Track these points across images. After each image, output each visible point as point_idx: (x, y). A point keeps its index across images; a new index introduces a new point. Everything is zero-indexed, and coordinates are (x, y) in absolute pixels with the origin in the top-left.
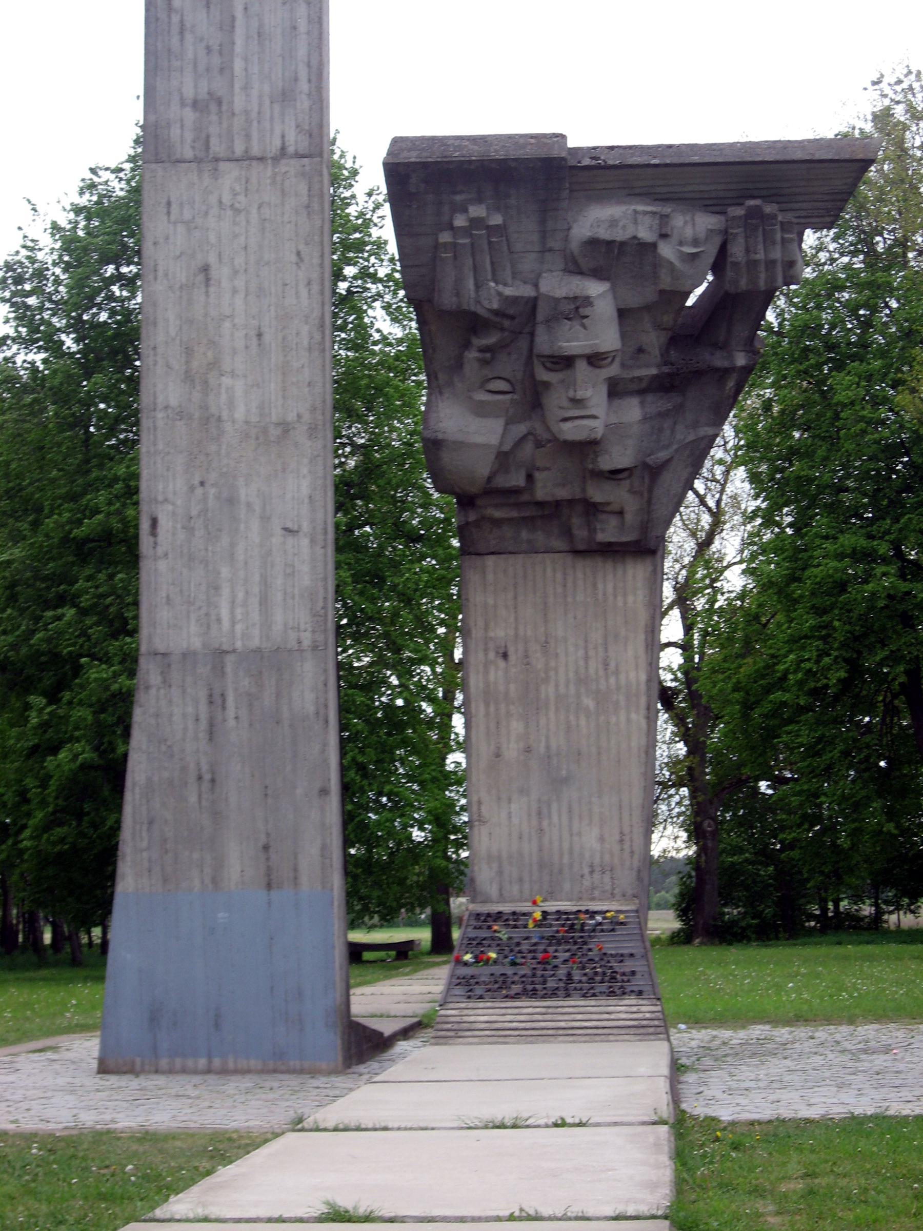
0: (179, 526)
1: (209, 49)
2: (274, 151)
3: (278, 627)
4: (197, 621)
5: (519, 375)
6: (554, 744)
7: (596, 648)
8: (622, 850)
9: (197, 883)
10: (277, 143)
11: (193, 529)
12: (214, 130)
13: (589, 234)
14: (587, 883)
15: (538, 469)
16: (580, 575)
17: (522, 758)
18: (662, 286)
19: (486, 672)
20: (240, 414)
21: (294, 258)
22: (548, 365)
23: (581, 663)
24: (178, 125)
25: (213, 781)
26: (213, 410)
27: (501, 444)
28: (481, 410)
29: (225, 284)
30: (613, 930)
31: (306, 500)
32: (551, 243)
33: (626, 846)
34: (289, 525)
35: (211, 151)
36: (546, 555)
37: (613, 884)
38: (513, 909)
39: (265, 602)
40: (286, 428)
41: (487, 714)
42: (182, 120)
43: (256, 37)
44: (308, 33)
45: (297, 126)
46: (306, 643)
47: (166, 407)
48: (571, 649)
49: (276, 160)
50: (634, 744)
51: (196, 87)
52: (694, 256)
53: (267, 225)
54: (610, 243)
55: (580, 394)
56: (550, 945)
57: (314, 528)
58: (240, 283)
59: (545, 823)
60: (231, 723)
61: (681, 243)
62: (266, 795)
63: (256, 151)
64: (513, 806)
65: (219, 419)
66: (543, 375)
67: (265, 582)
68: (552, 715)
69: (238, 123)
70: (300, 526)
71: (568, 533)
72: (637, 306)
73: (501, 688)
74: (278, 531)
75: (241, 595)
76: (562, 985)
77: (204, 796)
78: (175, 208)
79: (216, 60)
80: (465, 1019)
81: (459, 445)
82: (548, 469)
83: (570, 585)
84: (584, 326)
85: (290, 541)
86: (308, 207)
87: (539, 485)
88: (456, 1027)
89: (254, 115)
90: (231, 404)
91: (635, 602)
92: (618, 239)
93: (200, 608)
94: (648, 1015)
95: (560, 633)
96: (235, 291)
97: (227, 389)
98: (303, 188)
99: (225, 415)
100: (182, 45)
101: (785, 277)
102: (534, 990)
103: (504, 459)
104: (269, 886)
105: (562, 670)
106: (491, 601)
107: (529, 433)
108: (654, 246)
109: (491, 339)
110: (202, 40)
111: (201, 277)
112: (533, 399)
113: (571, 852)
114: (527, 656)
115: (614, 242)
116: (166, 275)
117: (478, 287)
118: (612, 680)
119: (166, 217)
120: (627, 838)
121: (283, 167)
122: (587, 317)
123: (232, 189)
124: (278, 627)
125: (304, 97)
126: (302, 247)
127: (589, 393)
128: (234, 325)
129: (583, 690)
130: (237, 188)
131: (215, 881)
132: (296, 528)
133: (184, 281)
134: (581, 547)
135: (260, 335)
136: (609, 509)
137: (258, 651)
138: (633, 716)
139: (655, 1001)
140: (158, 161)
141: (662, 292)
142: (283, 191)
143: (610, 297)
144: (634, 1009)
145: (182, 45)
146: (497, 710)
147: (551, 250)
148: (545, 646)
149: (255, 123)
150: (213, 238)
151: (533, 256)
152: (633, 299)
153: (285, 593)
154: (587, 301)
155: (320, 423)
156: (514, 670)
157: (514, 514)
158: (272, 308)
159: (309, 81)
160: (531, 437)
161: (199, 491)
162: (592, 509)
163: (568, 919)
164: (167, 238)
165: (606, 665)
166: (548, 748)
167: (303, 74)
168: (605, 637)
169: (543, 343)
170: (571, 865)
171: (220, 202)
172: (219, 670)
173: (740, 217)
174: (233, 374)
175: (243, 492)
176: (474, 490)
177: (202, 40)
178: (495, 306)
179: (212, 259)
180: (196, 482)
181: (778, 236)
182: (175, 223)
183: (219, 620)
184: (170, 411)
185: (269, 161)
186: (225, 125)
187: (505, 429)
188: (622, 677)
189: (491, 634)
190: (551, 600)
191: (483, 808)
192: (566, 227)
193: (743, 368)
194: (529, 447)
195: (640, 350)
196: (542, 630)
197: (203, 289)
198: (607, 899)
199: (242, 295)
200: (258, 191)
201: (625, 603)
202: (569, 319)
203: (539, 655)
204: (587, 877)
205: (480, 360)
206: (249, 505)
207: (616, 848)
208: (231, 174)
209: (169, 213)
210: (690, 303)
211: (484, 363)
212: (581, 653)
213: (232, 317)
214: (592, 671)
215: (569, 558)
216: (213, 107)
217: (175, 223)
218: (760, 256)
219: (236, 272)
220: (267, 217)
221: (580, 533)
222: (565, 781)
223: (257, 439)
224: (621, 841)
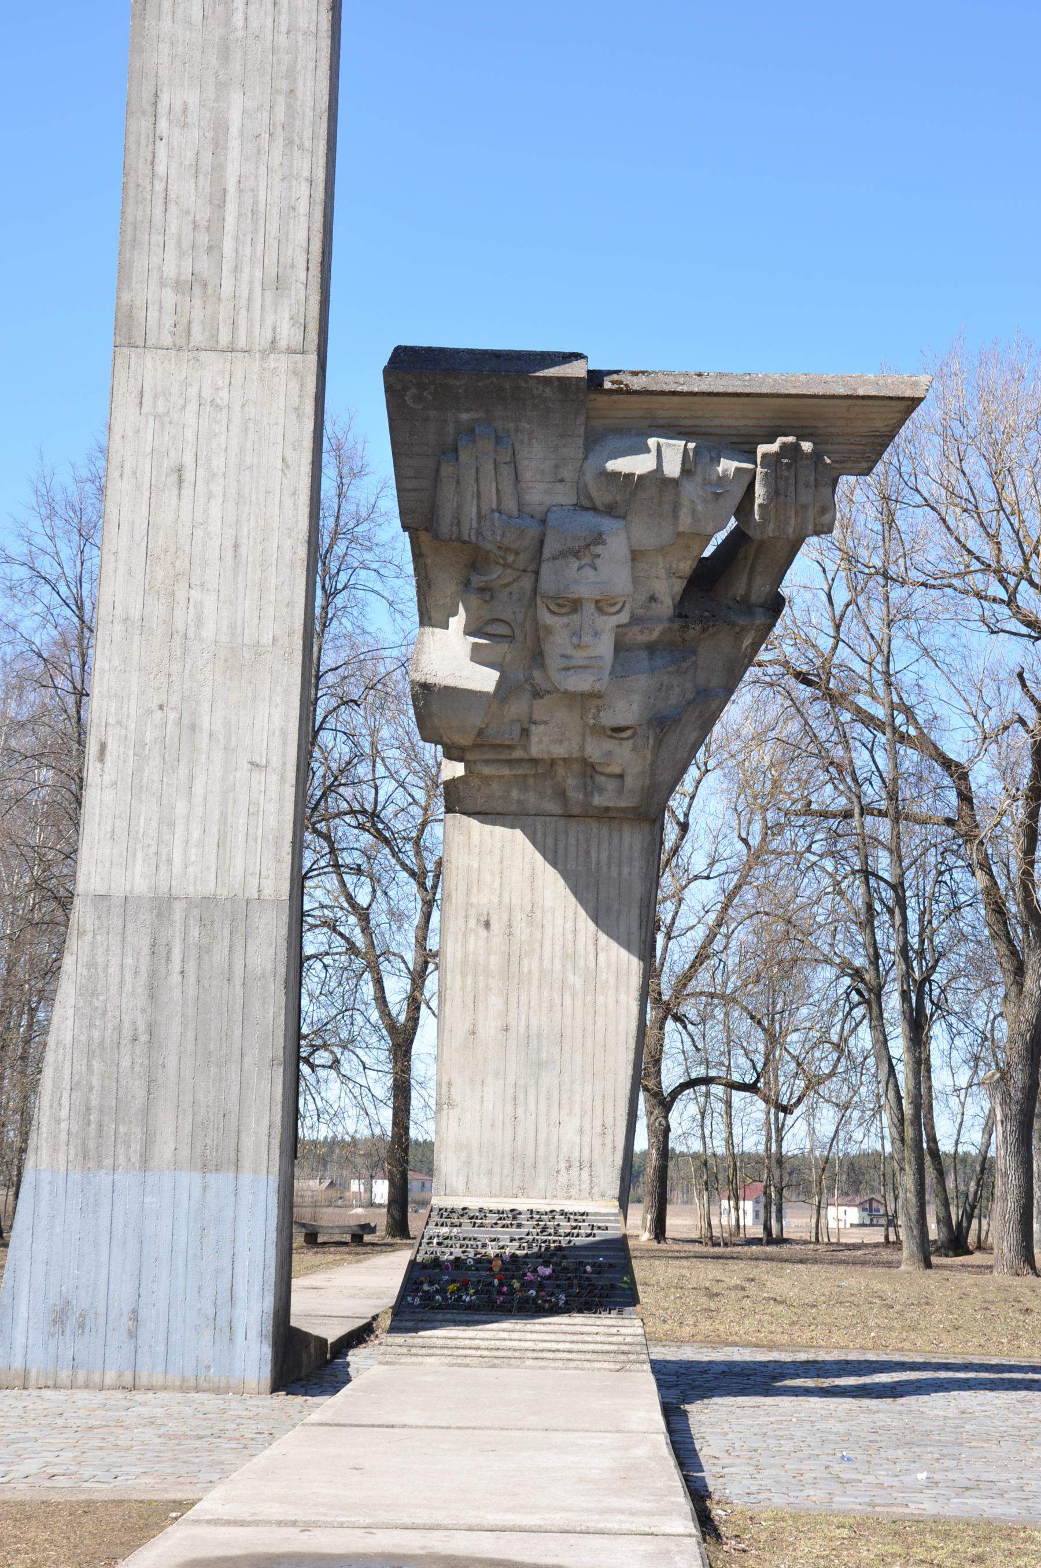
4: (144, 860)
5: (520, 617)
6: (534, 1024)
8: (603, 1144)
10: (269, 335)
12: (197, 315)
15: (535, 723)
17: (500, 1037)
21: (279, 464)
23: (570, 936)
34: (257, 759)
36: (537, 818)
38: (530, 1207)
41: (463, 987)
43: (249, 214)
49: (265, 354)
51: (179, 266)
59: (520, 1111)
63: (242, 342)
68: (534, 991)
75: (196, 834)
79: (203, 238)
82: (545, 723)
87: (534, 739)
89: (243, 302)
91: (630, 874)
93: (149, 846)
99: (191, 634)
120: (609, 1131)
126: (289, 453)
135: (236, 547)
138: (623, 997)
149: (243, 311)
161: (158, 715)
163: (540, 1220)
164: (138, 431)
170: (547, 1159)
175: (206, 719)
177: (188, 212)
179: (188, 459)
183: (170, 861)
186: (209, 311)
189: (474, 900)
191: (452, 1090)
199: (220, 501)
201: (620, 874)
203: (524, 925)
204: (563, 1172)
220: (252, 416)
223: (226, 661)
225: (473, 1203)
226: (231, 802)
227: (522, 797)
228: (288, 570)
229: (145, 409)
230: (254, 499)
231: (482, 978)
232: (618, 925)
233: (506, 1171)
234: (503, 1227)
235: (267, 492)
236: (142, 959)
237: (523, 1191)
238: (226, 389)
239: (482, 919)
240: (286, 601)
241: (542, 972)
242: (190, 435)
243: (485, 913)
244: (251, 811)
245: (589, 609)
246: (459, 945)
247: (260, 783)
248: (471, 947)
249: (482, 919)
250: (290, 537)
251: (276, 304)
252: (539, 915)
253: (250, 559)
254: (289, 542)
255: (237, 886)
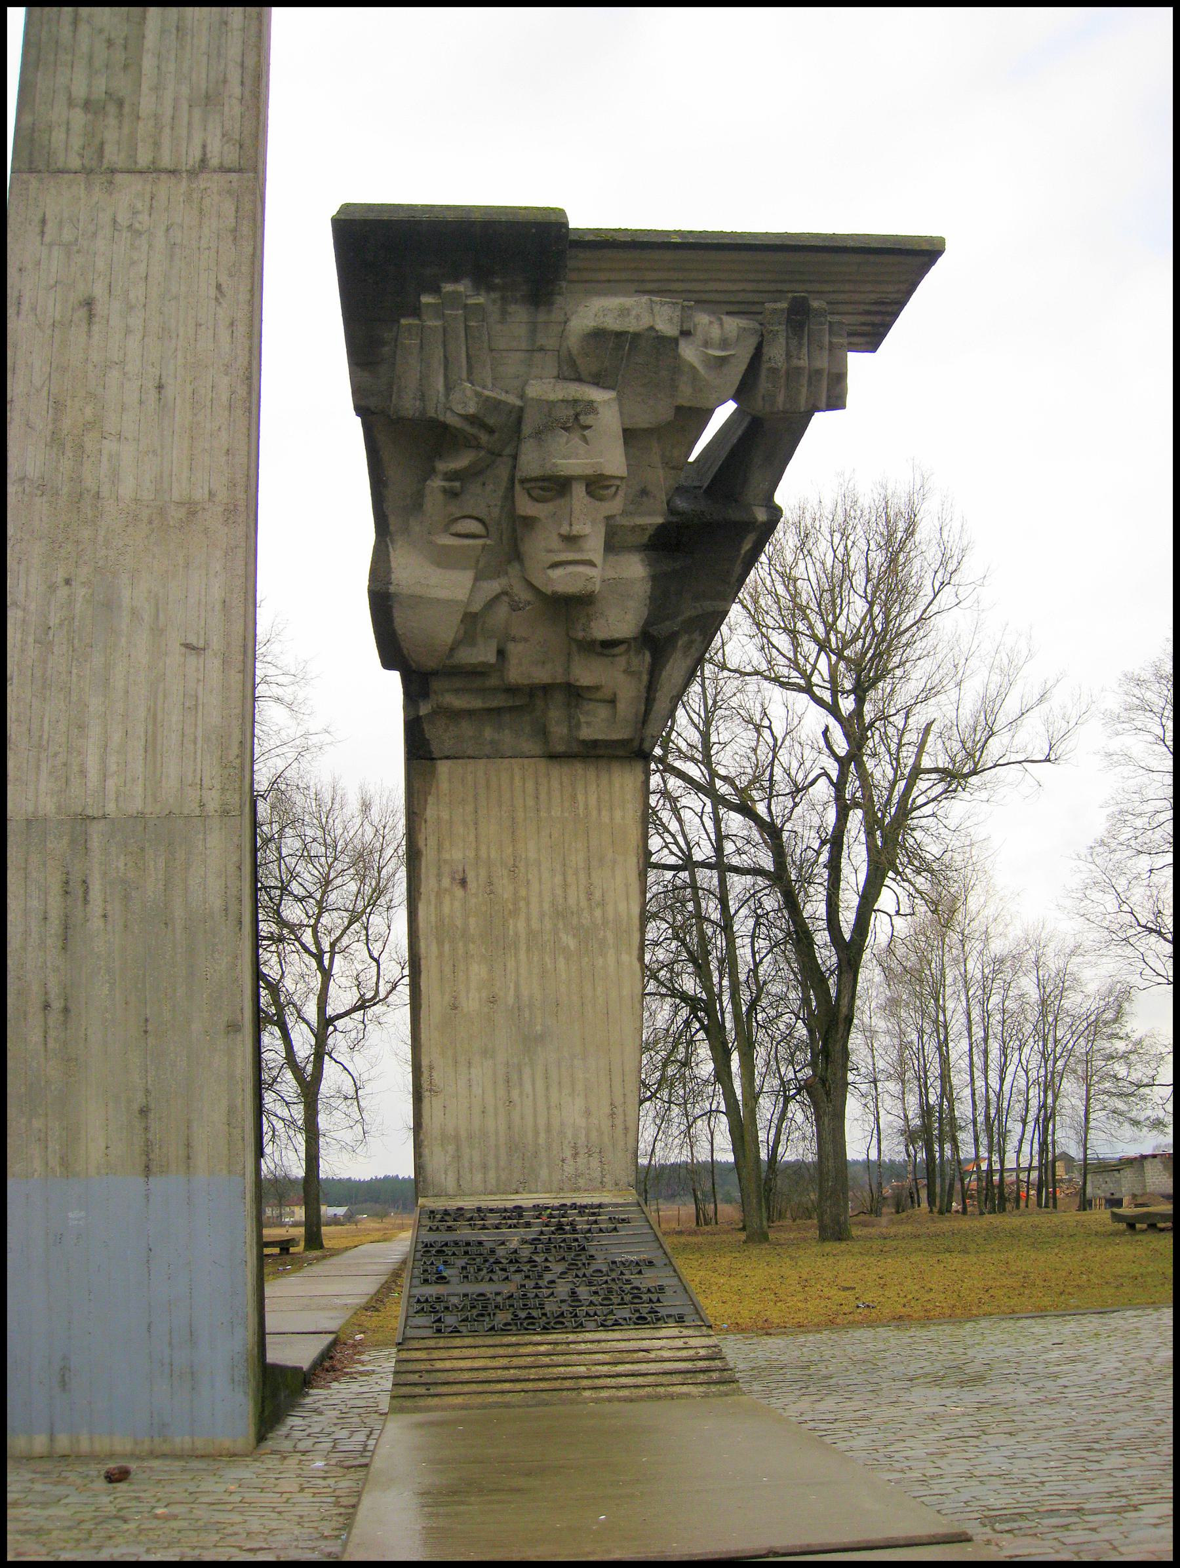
0: (31, 640)
1: (110, 43)
2: (191, 163)
3: (170, 784)
4: (50, 773)
5: (496, 512)
6: (525, 992)
7: (576, 874)
9: (37, 1164)
10: (198, 154)
11: (51, 643)
12: (111, 136)
13: (592, 324)
14: (569, 1169)
15: (514, 639)
16: (555, 784)
17: (486, 1010)
18: (681, 402)
19: (439, 903)
20: (127, 489)
21: (213, 292)
22: (535, 493)
23: (559, 892)
24: (63, 129)
25: (66, 1010)
26: (89, 483)
27: (469, 603)
28: (444, 559)
29: (115, 321)
30: (615, 1229)
31: (218, 607)
32: (542, 341)
33: (619, 1122)
34: (193, 640)
35: (105, 161)
36: (513, 761)
37: (603, 1169)
38: (477, 1204)
39: (151, 746)
40: (192, 509)
41: (441, 955)
42: (68, 123)
43: (174, 31)
44: (243, 30)
45: (223, 136)
46: (212, 806)
47: (22, 480)
48: (546, 875)
49: (193, 173)
50: (626, 992)
51: (89, 86)
52: (723, 361)
53: (177, 251)
54: (620, 335)
55: (577, 529)
56: (535, 1252)
57: (229, 644)
58: (135, 321)
59: (515, 1093)
60: (97, 923)
61: (706, 344)
62: (146, 1032)
63: (166, 161)
64: (473, 1070)
65: (98, 496)
66: (526, 506)
67: (153, 716)
68: (523, 956)
69: (144, 128)
70: (207, 643)
71: (543, 733)
72: (646, 426)
73: (459, 923)
74: (176, 648)
75: (116, 738)
76: (565, 1307)
77: (52, 1033)
78: (50, 227)
79: (119, 56)
80: (439, 1365)
81: (418, 601)
82: (526, 640)
83: (543, 796)
84: (585, 440)
85: (192, 660)
86: (235, 230)
87: (513, 661)
88: (427, 1378)
89: (166, 120)
90: (115, 477)
91: (623, 818)
92: (631, 330)
93: (56, 755)
94: (702, 1352)
95: (532, 855)
96: (128, 331)
97: (111, 456)
98: (228, 207)
99: (105, 492)
100: (74, 37)
101: (829, 397)
102: (529, 1317)
103: (471, 619)
104: (147, 1170)
105: (534, 900)
106: (445, 816)
107: (505, 593)
108: (675, 341)
109: (461, 461)
110: (101, 31)
111: (82, 313)
112: (510, 541)
113: (548, 1130)
114: (491, 884)
115: (627, 332)
116: (34, 309)
117: (448, 389)
118: (598, 913)
119: (39, 238)
120: (619, 1111)
121: (203, 181)
122: (589, 427)
123: (132, 207)
124: (170, 784)
125: (235, 102)
126: (223, 278)
127: (587, 530)
128: (125, 374)
129: (561, 925)
130: (139, 206)
131: (64, 1162)
132: (201, 645)
133: (58, 318)
134: (560, 748)
135: (160, 387)
136: (599, 695)
137: (141, 816)
138: (625, 958)
139: (705, 1330)
140: (31, 171)
141: (679, 409)
142: (201, 211)
143: (615, 407)
144: (679, 1343)
145: (74, 37)
146: (454, 950)
147: (541, 349)
148: (513, 870)
149: (167, 130)
150: (101, 265)
151: (519, 356)
152: (644, 419)
153: (183, 735)
154: (590, 407)
155: (242, 503)
156: (474, 900)
157: (477, 703)
158: (180, 354)
159: (242, 83)
160: (505, 598)
161: (63, 592)
162: (575, 694)
163: (551, 1216)
164: (39, 263)
165: (589, 895)
166: (517, 997)
167: (234, 76)
168: (588, 860)
169: (531, 461)
170: (549, 1149)
171: (115, 221)
172: (79, 844)
173: (782, 310)
174: (119, 437)
175: (126, 593)
176: (431, 664)
177: (101, 31)
178: (472, 410)
179: (99, 291)
180: (60, 578)
181: (826, 339)
182: (51, 245)
183: (83, 773)
184: (27, 483)
185: (184, 175)
186: (126, 130)
187: (474, 585)
188: (610, 909)
189: (446, 856)
190: (520, 815)
191: (434, 1074)
192: (562, 318)
193: (764, 524)
194: (502, 611)
195: (644, 492)
196: (510, 850)
197: (85, 328)
198: (594, 1190)
199: (139, 337)
200: (166, 209)
201: (612, 819)
202: (566, 429)
203: (505, 881)
204: (570, 1161)
205: (445, 491)
206: (134, 612)
207: (606, 1124)
208: (130, 189)
209: (43, 233)
210: (691, 459)
211: (452, 494)
212: (558, 879)
213: (122, 363)
214: (572, 901)
215: (542, 764)
216: (112, 109)
217: (51, 245)
218: (803, 363)
219: (131, 308)
220: (178, 241)
221: (559, 731)
222: (540, 1039)
223: (150, 522)
224: (612, 1115)
225: (469, 1203)
226: (160, 695)
227: (496, 737)
228: (226, 413)
229: (47, 239)
230: (181, 333)
231: (461, 944)
232: (614, 877)
233: (502, 1163)
234: (510, 1227)
235: (198, 325)
236: (50, 900)
237: (523, 1186)
238: (146, 213)
239: (457, 877)
240: (225, 448)
241: (530, 932)
242: (101, 265)
243: (461, 869)
244: (187, 705)
245: (579, 490)
246: (432, 908)
247: (198, 670)
248: (446, 910)
249: (457, 877)
250: (226, 374)
251: (205, 121)
252: (523, 870)
253: (178, 401)
254: (225, 380)
255: (171, 800)
